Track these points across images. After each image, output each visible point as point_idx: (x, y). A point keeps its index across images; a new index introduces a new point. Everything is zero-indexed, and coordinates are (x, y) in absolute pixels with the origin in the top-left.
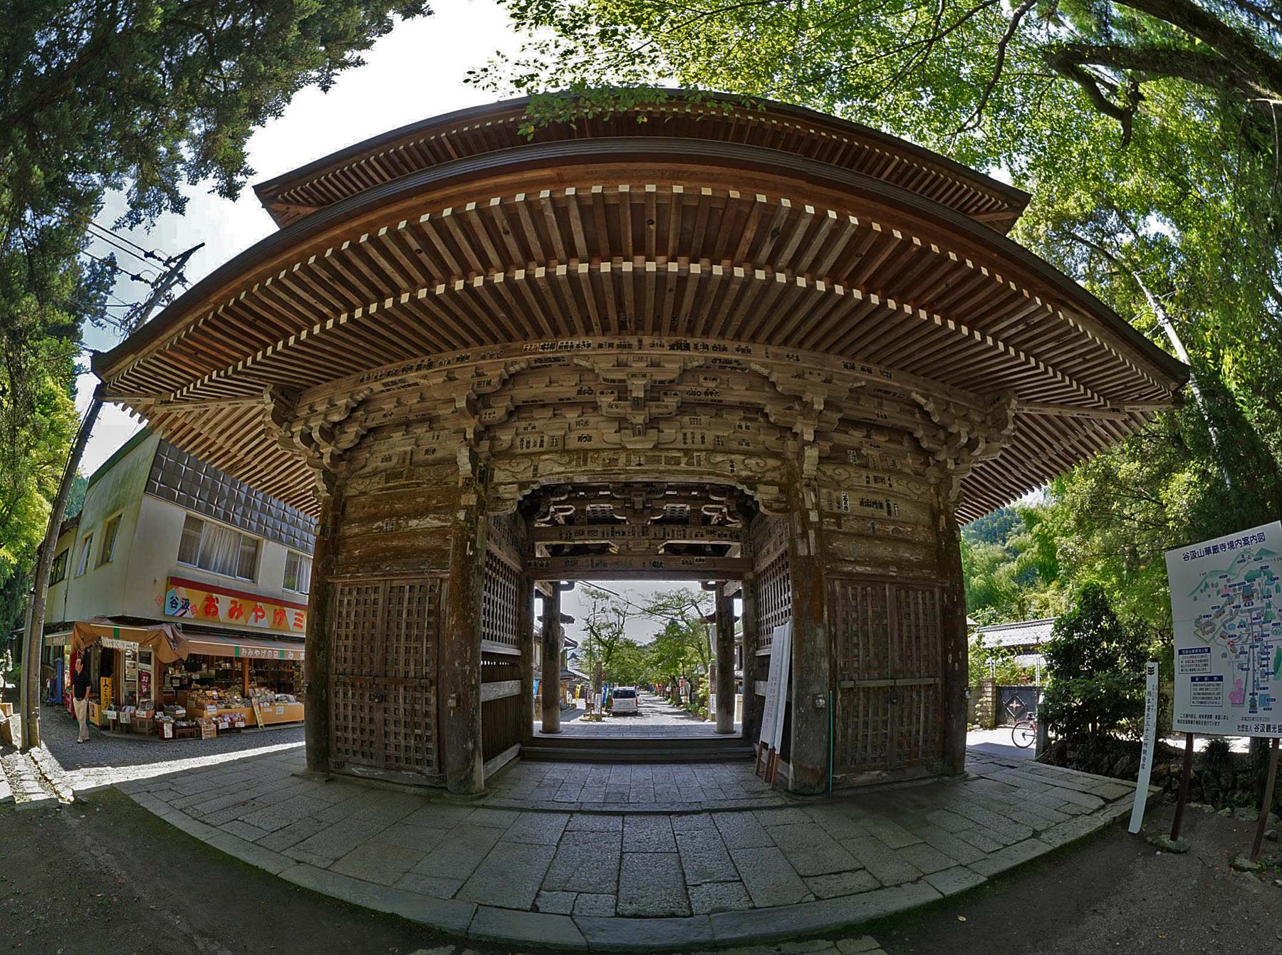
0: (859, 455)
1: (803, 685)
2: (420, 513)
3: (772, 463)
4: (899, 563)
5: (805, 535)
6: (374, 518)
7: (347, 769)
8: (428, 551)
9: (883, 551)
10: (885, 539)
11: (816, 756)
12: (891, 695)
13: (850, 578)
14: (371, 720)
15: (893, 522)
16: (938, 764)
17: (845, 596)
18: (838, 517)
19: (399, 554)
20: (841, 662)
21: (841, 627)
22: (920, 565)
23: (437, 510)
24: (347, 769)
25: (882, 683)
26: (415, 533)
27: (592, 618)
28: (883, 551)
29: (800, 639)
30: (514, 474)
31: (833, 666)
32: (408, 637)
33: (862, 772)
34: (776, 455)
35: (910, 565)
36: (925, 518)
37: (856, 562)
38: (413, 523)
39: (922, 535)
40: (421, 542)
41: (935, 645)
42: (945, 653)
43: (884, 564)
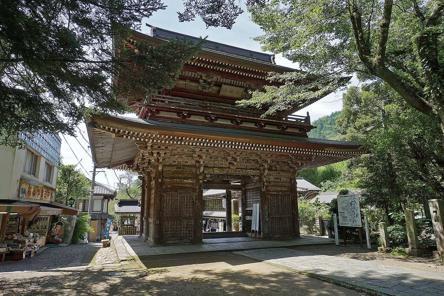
0: (275, 167)
1: (263, 216)
2: (187, 179)
3: (258, 171)
4: (281, 191)
5: (263, 187)
6: (173, 178)
7: (167, 242)
8: (190, 188)
9: (278, 189)
10: (279, 186)
11: (266, 231)
12: (280, 219)
13: (272, 195)
14: (177, 228)
15: (281, 182)
16: (293, 234)
17: (270, 198)
18: (269, 182)
19: (182, 188)
20: (270, 212)
21: (270, 205)
22: (287, 191)
23: (191, 178)
24: (167, 242)
25: (278, 216)
26: (186, 183)
27: (128, 185)
28: (278, 189)
29: (262, 208)
30: (209, 172)
31: (269, 212)
32: (187, 208)
33: (276, 235)
34: (259, 170)
35: (285, 191)
36: (289, 180)
37: (273, 192)
38: (185, 181)
39: (288, 184)
40: (187, 185)
41: (290, 208)
42: (292, 210)
43: (279, 191)
